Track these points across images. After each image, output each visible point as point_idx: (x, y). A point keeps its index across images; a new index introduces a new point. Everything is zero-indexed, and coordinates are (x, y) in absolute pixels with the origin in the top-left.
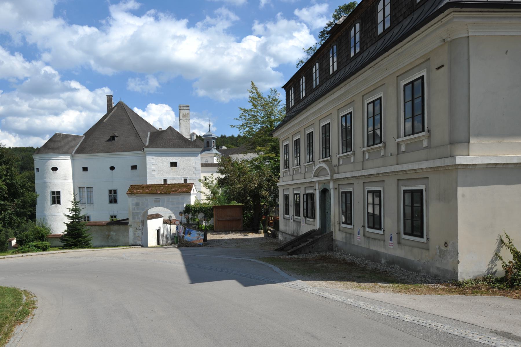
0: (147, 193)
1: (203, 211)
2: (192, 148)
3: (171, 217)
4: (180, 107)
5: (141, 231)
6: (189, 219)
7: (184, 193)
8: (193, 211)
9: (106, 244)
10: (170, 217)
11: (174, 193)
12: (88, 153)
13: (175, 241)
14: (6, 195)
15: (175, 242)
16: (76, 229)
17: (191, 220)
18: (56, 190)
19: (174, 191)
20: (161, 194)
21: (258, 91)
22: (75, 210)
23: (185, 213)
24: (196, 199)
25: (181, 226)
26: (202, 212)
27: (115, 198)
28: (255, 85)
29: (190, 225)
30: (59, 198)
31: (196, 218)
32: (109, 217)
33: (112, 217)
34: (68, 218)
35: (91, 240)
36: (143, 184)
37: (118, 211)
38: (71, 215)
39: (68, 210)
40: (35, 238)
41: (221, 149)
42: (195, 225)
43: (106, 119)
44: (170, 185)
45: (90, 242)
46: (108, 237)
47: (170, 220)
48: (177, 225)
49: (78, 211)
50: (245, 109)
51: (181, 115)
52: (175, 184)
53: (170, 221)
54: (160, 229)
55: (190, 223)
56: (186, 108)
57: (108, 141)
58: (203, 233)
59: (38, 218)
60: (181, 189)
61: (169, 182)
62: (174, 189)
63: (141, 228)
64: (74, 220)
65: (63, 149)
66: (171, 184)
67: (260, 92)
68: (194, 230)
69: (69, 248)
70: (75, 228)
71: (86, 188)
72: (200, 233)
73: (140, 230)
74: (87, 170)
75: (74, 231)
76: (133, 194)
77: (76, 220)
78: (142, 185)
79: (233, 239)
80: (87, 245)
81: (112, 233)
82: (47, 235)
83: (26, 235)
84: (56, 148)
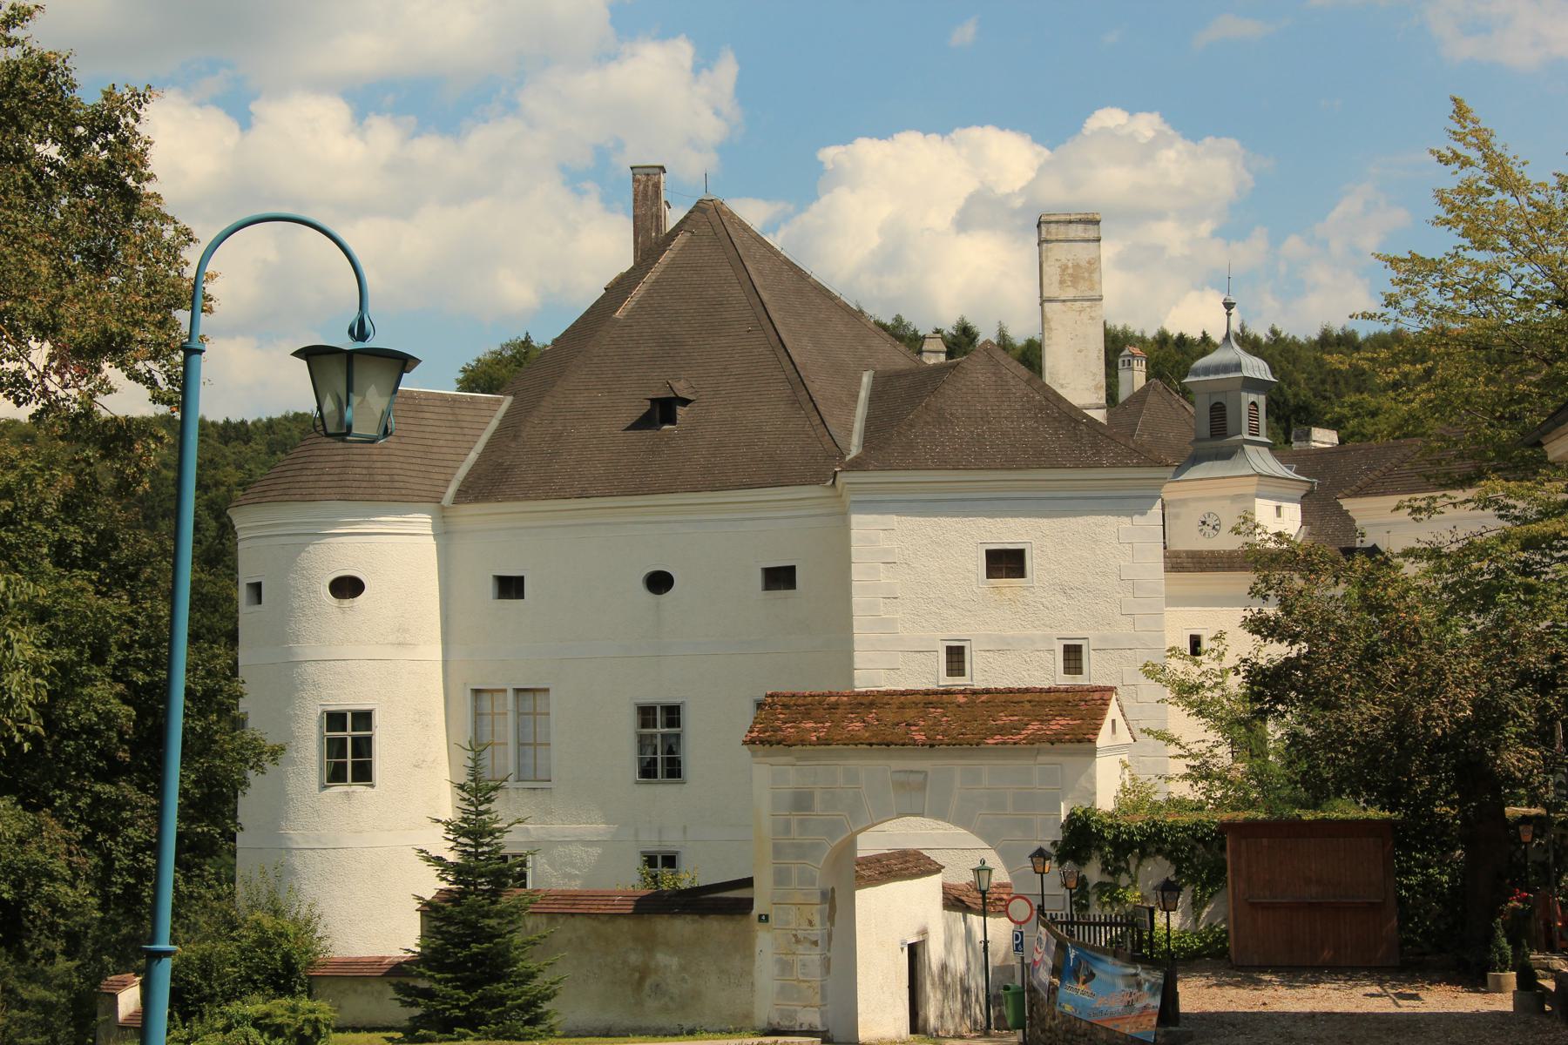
0: (854, 741)
1: (1167, 847)
2: (1113, 466)
3: (990, 871)
4: (1043, 227)
5: (818, 950)
6: (1089, 888)
7: (1060, 741)
8: (1111, 843)
9: (628, 1022)
10: (982, 870)
11: (1004, 743)
12: (527, 498)
13: (1009, 1013)
14: (121, 754)
15: (1010, 1022)
16: (480, 935)
17: (1099, 898)
18: (348, 701)
19: (1001, 730)
20: (932, 746)
21: (1498, 149)
22: (472, 830)
23: (1061, 860)
24: (1127, 777)
25: (1042, 928)
26: (1159, 851)
27: (670, 751)
28: (1476, 114)
29: (1089, 924)
30: (363, 747)
31: (1126, 888)
32: (638, 861)
33: (651, 860)
34: (438, 876)
35: (555, 995)
36: (834, 690)
37: (685, 830)
38: (452, 857)
39: (442, 829)
40: (248, 979)
41: (1303, 445)
42: (1121, 925)
43: (629, 303)
44: (984, 698)
45: (546, 1006)
46: (642, 979)
47: (984, 887)
48: (1019, 923)
49: (491, 834)
50: (1414, 258)
51: (1052, 271)
52: (1010, 691)
53: (984, 893)
54: (923, 942)
55: (1095, 911)
56: (1077, 231)
57: (634, 427)
58: (1157, 977)
59: (246, 863)
60: (1042, 722)
61: (983, 673)
62: (1004, 719)
63: (817, 931)
64: (467, 884)
65: (396, 478)
66: (987, 691)
67: (1509, 155)
68: (1110, 959)
69: (439, 1036)
70: (473, 926)
71: (510, 694)
72: (1143, 975)
73: (815, 943)
74: (519, 594)
75: (466, 946)
76: (779, 743)
77: (481, 884)
78: (831, 694)
79: (1329, 1016)
80: (531, 1022)
81: (662, 958)
82: (311, 963)
83: (202, 959)
84: (358, 471)
